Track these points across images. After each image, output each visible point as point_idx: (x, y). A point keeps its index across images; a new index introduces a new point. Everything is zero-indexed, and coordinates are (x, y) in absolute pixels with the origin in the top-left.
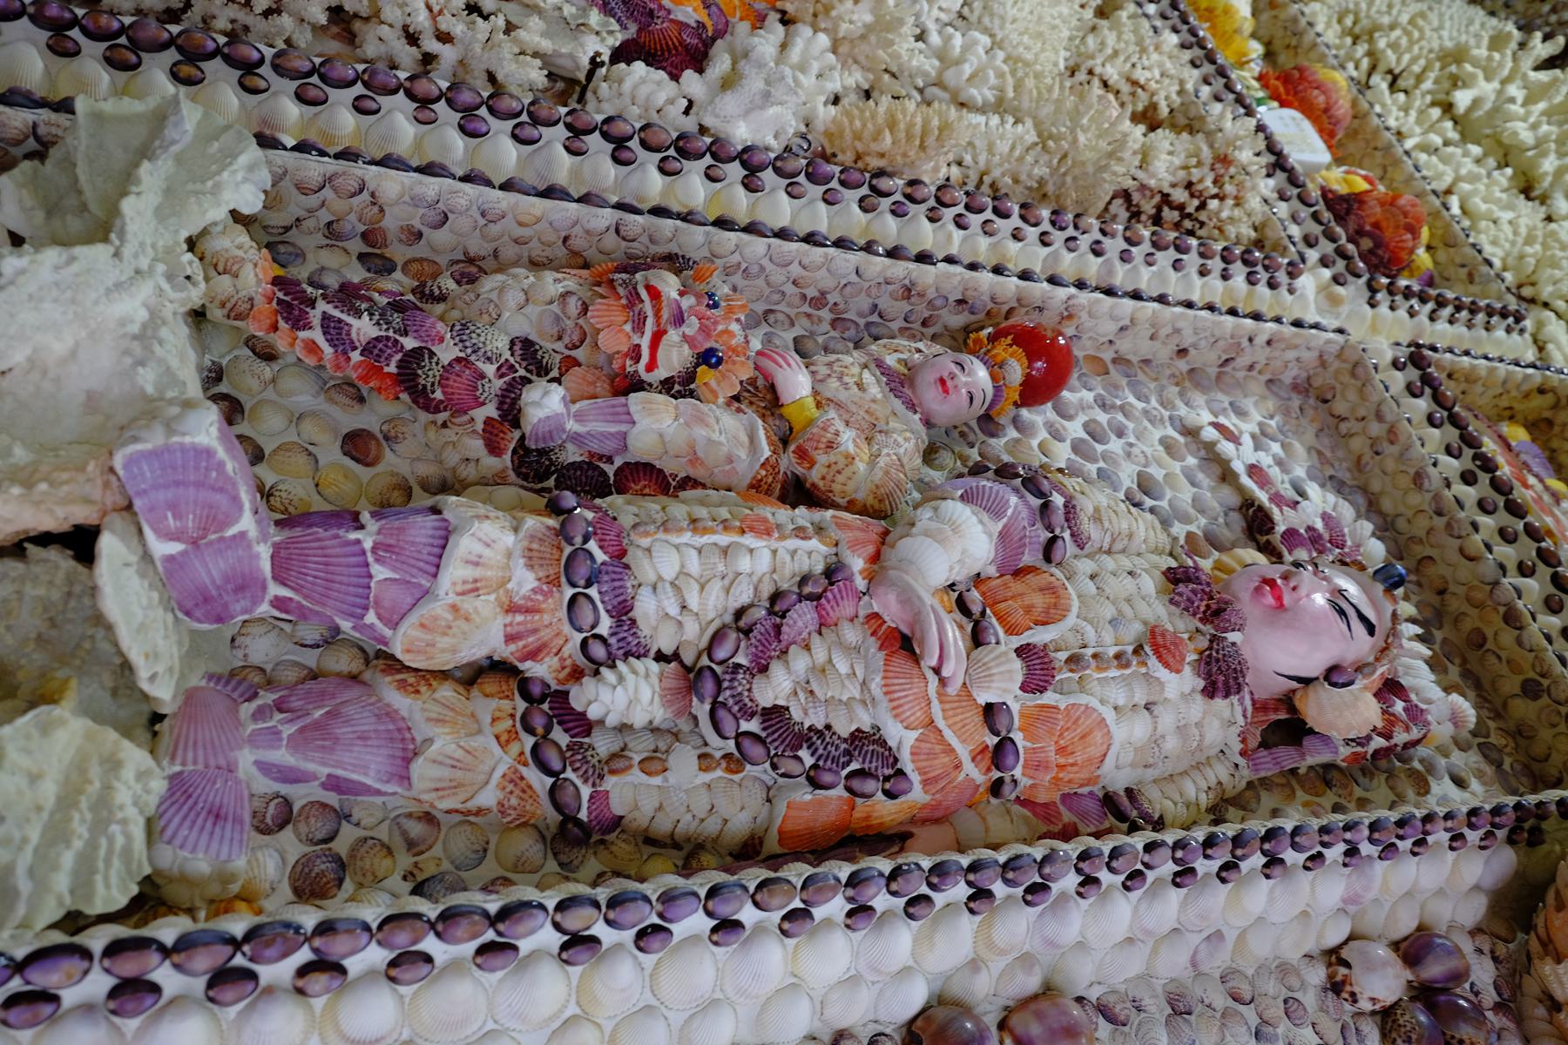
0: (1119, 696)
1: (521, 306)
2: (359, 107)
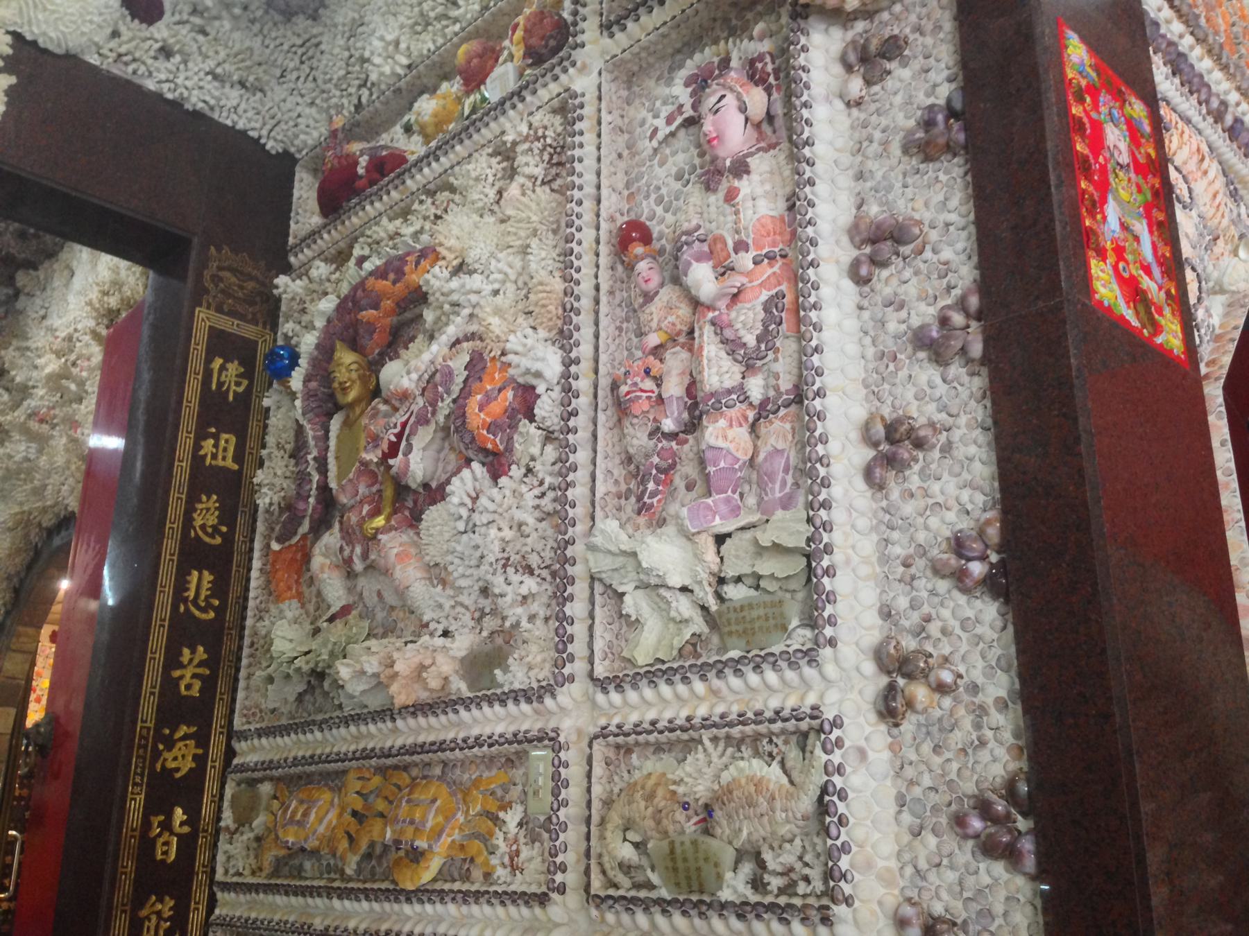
1: (639, 439)
2: (573, 506)
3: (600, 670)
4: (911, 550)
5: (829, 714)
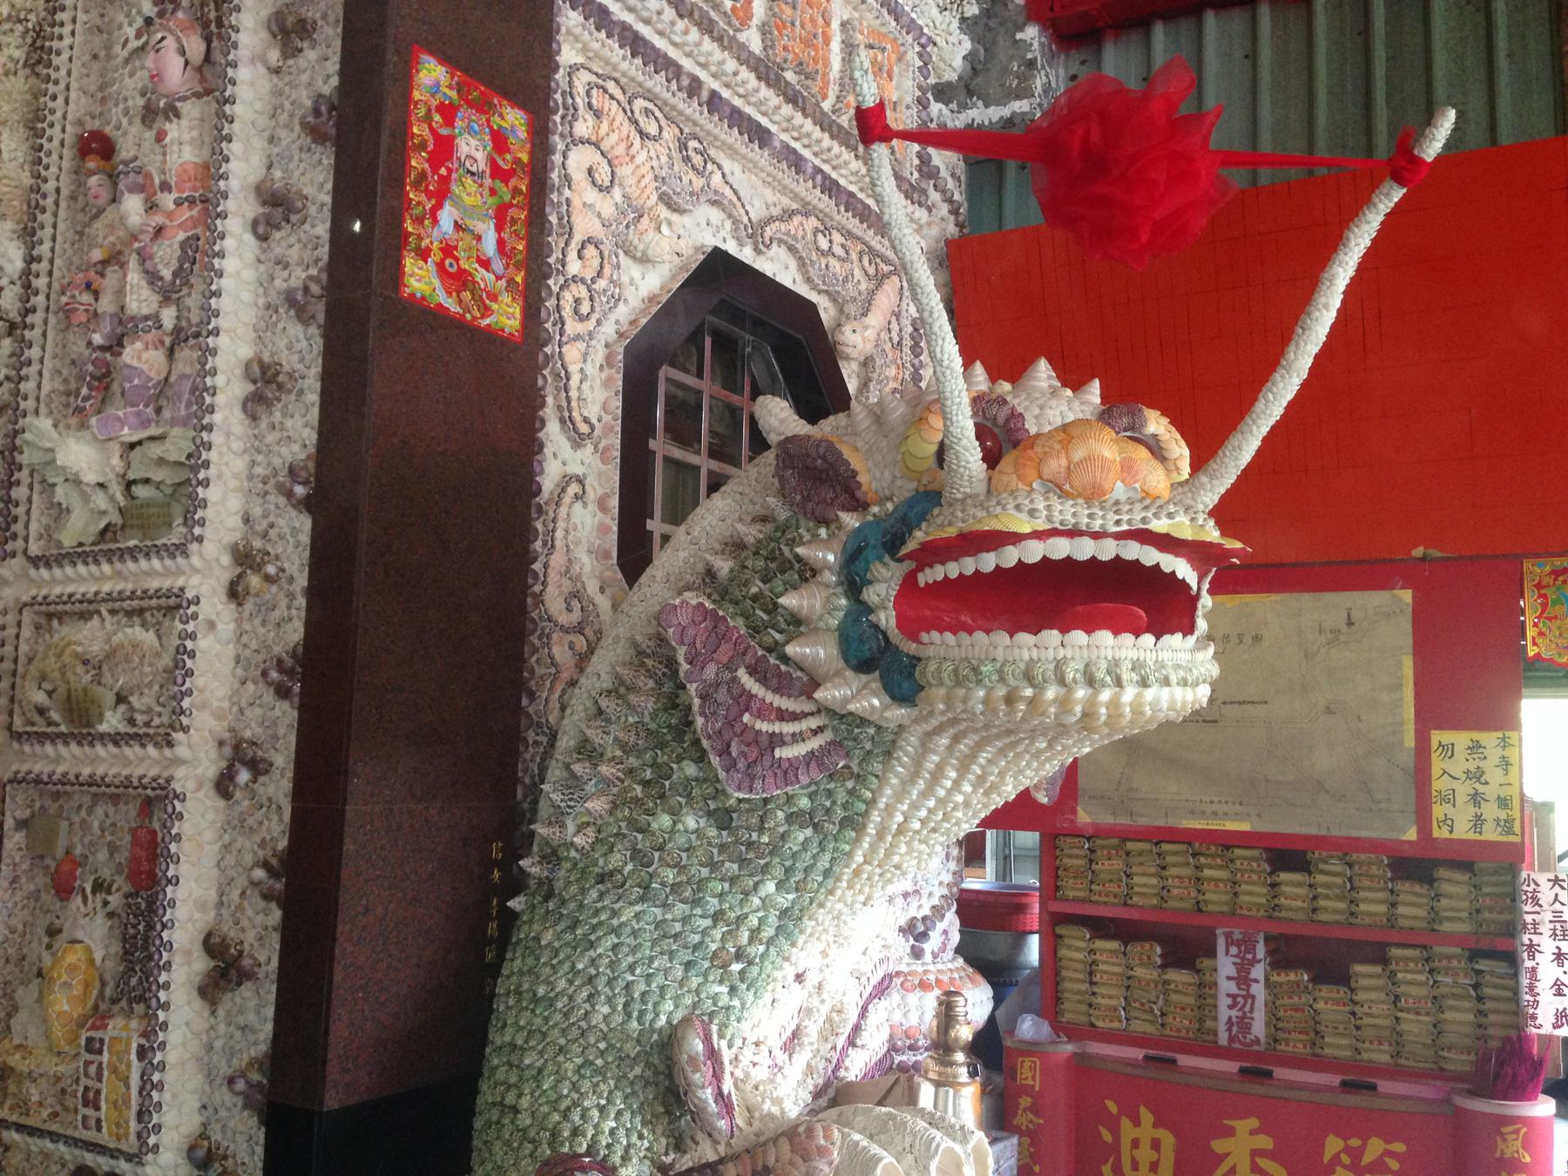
0: (175, 156)
3: (34, 549)
5: (190, 594)
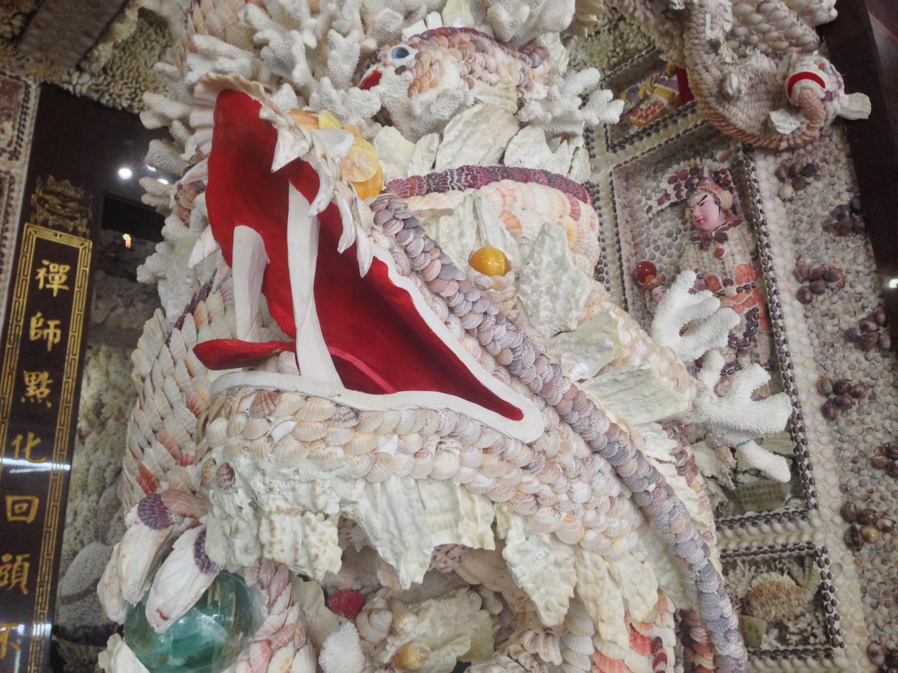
0: (731, 263)
4: (857, 454)
5: (819, 546)
